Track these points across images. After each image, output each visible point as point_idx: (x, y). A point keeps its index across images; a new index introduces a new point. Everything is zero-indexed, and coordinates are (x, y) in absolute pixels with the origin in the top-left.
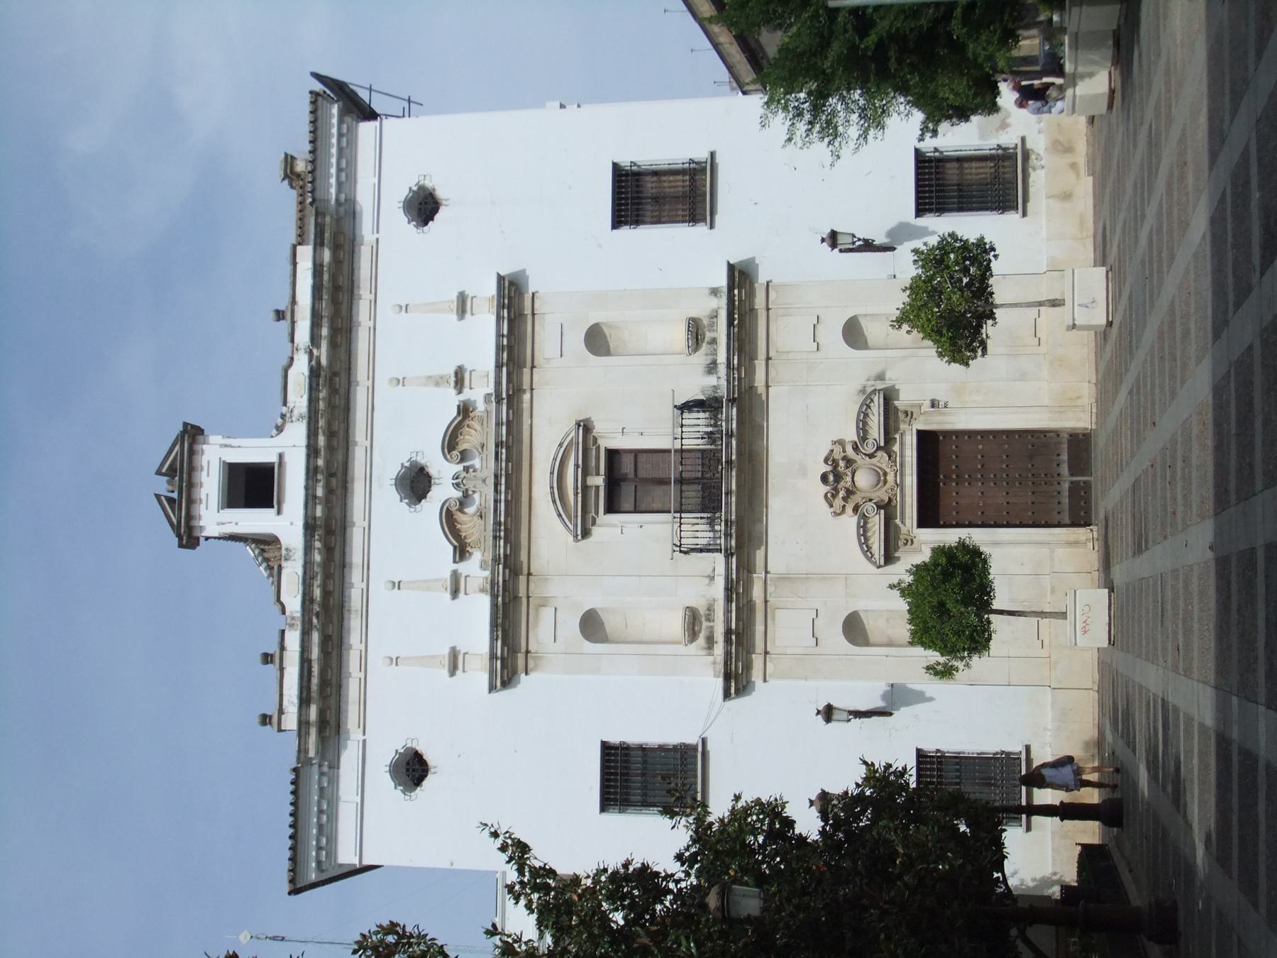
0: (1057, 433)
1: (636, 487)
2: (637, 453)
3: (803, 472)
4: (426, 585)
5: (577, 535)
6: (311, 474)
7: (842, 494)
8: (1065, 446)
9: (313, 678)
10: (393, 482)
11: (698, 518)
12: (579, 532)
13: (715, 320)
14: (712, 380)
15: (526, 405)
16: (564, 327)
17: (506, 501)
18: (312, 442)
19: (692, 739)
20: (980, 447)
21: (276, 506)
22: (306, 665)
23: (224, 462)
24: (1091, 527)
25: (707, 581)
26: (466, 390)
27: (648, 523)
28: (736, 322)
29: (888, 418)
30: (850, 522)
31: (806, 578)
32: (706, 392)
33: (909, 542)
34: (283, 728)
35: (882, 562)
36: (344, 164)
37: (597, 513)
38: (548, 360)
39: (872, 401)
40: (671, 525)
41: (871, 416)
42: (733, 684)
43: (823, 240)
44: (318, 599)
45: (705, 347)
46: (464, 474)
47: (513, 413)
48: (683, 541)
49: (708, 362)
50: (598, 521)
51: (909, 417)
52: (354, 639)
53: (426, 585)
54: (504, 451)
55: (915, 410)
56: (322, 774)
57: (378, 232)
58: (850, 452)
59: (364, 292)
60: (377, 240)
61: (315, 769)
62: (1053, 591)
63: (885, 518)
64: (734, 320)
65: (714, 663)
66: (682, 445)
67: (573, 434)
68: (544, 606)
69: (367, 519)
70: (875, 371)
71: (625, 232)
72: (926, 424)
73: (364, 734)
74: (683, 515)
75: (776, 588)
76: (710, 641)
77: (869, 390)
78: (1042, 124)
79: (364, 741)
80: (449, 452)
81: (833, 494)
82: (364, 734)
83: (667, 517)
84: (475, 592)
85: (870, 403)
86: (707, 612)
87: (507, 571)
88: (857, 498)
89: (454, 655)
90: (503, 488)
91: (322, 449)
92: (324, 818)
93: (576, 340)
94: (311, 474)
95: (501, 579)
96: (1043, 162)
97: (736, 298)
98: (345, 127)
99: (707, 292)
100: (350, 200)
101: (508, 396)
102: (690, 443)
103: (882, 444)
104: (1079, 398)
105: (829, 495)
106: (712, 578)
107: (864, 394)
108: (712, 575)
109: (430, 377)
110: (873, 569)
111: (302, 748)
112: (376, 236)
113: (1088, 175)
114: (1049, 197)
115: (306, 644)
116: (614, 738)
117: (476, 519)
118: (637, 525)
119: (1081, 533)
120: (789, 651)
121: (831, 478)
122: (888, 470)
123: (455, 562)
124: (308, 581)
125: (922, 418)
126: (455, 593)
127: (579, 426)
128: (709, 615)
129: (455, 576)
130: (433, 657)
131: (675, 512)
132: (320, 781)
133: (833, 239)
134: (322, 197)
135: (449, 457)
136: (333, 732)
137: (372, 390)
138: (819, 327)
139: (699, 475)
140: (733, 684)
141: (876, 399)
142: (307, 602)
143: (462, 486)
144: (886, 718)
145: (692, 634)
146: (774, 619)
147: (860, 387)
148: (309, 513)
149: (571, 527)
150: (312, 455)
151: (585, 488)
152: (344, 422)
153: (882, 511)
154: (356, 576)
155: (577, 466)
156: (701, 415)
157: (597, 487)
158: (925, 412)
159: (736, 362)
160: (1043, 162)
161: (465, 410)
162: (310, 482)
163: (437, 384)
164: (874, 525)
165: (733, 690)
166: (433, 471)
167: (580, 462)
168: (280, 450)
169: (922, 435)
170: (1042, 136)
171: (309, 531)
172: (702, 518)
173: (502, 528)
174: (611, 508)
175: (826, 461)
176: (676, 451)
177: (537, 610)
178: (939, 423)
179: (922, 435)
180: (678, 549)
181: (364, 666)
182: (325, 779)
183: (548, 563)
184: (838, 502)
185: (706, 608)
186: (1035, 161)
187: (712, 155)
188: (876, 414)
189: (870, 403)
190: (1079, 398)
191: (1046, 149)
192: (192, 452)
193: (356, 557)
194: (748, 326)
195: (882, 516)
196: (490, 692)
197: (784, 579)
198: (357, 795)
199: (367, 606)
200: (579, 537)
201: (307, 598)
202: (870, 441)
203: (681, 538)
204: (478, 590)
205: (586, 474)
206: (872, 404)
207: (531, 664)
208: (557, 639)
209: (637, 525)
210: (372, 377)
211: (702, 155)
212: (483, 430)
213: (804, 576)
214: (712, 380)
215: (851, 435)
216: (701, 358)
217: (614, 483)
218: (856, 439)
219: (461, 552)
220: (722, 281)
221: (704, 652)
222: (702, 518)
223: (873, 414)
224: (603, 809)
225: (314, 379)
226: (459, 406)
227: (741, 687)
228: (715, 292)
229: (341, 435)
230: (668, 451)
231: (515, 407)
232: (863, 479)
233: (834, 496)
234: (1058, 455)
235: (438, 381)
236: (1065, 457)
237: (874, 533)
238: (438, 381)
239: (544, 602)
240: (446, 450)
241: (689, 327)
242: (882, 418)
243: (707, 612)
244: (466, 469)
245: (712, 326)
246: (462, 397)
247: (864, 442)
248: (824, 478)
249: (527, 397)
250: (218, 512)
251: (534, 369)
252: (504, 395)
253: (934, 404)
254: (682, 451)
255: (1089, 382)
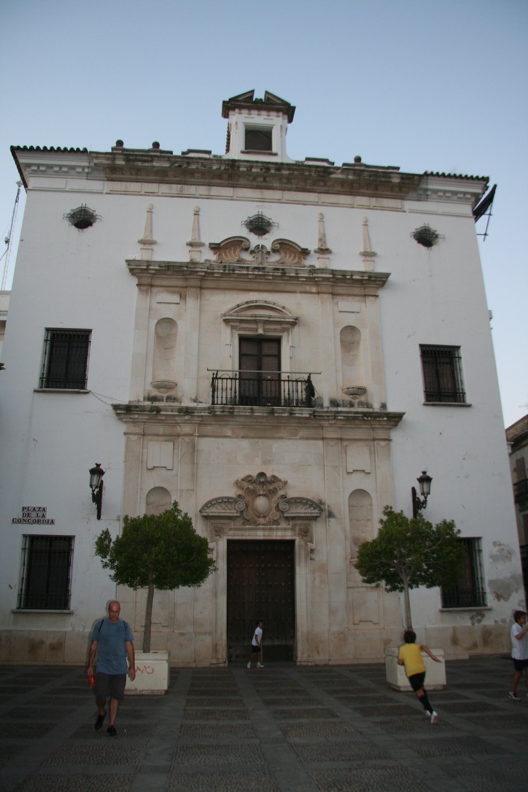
0: (293, 636)
1: (257, 356)
2: (278, 356)
3: (266, 462)
4: (197, 228)
5: (225, 316)
6: (265, 165)
7: (251, 487)
8: (284, 643)
9: (141, 163)
10: (260, 213)
11: (235, 390)
12: (227, 317)
13: (365, 406)
14: (326, 404)
15: (308, 288)
16: (357, 314)
17: (248, 274)
18: (285, 166)
19: (89, 386)
20: (283, 584)
21: (246, 151)
22: (149, 159)
23: (272, 127)
24: (227, 662)
25: (194, 398)
26: (318, 255)
27: (233, 360)
28: (365, 418)
29: (303, 520)
30: (232, 493)
31: (194, 463)
32: (319, 400)
33: (217, 534)
34: (221, 403)
35: (205, 514)
36: (448, 195)
37: (240, 329)
38: (337, 303)
39: (315, 508)
40: (231, 369)
41: (304, 508)
42: (123, 412)
43: (424, 473)
44: (189, 167)
45: (348, 398)
46: (265, 251)
47: (303, 281)
48: (220, 381)
49: (338, 402)
50: (234, 331)
51: (304, 534)
52: (164, 188)
53: (197, 228)
54: (280, 274)
55: (308, 538)
56: (83, 168)
57: (410, 212)
58: (281, 493)
59: (373, 201)
60: (405, 212)
61: (86, 164)
62: (182, 634)
63: (234, 516)
64: (367, 417)
65: (139, 401)
66: (284, 381)
67: (290, 315)
68: (181, 297)
69: (237, 198)
70: (335, 511)
71: (417, 353)
72: (299, 546)
73: (106, 193)
74: (237, 381)
75: (188, 443)
76: (154, 399)
77: (322, 506)
78: (501, 623)
79: (102, 193)
80: (279, 243)
81: (251, 481)
82: (106, 193)
83: (237, 367)
84: (191, 257)
85: (313, 507)
86: (173, 398)
87: (203, 274)
88: (248, 498)
89: (152, 243)
90: (256, 273)
91: (280, 173)
92: (57, 169)
93: (350, 320)
94: (265, 165)
95: (199, 270)
96: (476, 624)
97: (381, 419)
98: (468, 196)
99: (383, 402)
100: (427, 198)
101: (315, 278)
102: (285, 387)
103: (285, 515)
104: (318, 652)
105: (250, 478)
106: (195, 401)
107: (320, 503)
108: (197, 401)
109: (324, 236)
110: (200, 507)
111: (99, 155)
112: (408, 211)
113: (470, 656)
114: (454, 629)
115: (162, 159)
116: (93, 338)
117: (237, 258)
118: (231, 354)
119: (223, 654)
120: (145, 451)
121: (262, 480)
122: (267, 519)
123: (210, 244)
124: (200, 161)
125: (303, 543)
126: (191, 244)
127: (296, 319)
128: (171, 399)
129: (202, 245)
130: (151, 232)
131: (240, 373)
132: (79, 167)
133: (425, 479)
134: (429, 181)
135: (276, 243)
136: (109, 176)
137: (316, 204)
138: (362, 474)
139: (265, 395)
140: (123, 412)
141: (316, 511)
142: (187, 160)
143: (258, 250)
144: (96, 515)
145: (158, 386)
146: (167, 441)
147: (323, 501)
148: (242, 163)
149: (231, 312)
150: (277, 167)
151: (255, 322)
152: (296, 188)
153: (238, 515)
154: (202, 190)
155: (270, 317)
156: (304, 396)
157: (257, 330)
158: (307, 545)
159: (340, 418)
160: (476, 624)
161: (305, 252)
162: (260, 165)
163: (320, 240)
164: (229, 509)
165: (119, 411)
166: (266, 236)
167: (271, 319)
168: (279, 153)
169: (292, 543)
170: (493, 623)
171: (230, 163)
172: (235, 392)
173: (231, 272)
174: (242, 339)
175: (274, 477)
176: (280, 375)
177: (178, 292)
178: (300, 555)
179: (292, 543)
180: (215, 376)
181: (148, 194)
182: (80, 170)
183: (207, 300)
184: (246, 485)
185: (175, 396)
186: (477, 619)
187: (469, 406)
188: (306, 511)
189: (309, 504)
190: (318, 652)
191: (485, 626)
192: (278, 110)
193: (215, 191)
194: (363, 426)
195: (235, 515)
196: (127, 261)
197: (193, 447)
198: (70, 189)
199: (185, 197)
200: (224, 318)
201: (190, 161)
202: (287, 506)
203: (222, 379)
204: (192, 258)
205: (266, 322)
206: (312, 508)
207: (143, 288)
208: (159, 305)
209: (231, 354)
210: (323, 204)
211: (468, 400)
212: (293, 264)
213: (195, 461)
214: (326, 404)
215: (292, 494)
216: (341, 396)
217: (260, 340)
218: (288, 497)
219: (215, 248)
220: (392, 409)
221: (146, 395)
222: (235, 392)
223: (305, 509)
224: (48, 330)
225: (322, 169)
226: (307, 249)
227: (122, 417)
228: (384, 406)
229: (289, 186)
230: (279, 368)
231: (307, 283)
232: (261, 503)
233: (250, 481)
234: (277, 638)
235: (322, 239)
236: (277, 643)
237: (224, 509)
238: (322, 239)
239: (183, 297)
240: (280, 242)
241: (361, 389)
242: (303, 515)
243: (173, 398)
244: (268, 253)
245: (361, 404)
246: (312, 253)
247: (287, 502)
248: (262, 474)
249: (314, 290)
250: (243, 123)
251: (331, 296)
252: (315, 275)
253: (312, 551)
254: (280, 380)
255: (329, 660)
